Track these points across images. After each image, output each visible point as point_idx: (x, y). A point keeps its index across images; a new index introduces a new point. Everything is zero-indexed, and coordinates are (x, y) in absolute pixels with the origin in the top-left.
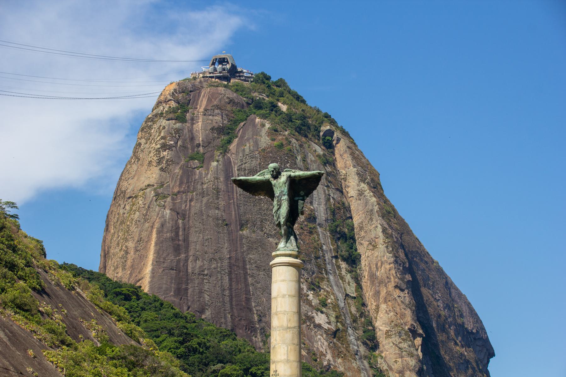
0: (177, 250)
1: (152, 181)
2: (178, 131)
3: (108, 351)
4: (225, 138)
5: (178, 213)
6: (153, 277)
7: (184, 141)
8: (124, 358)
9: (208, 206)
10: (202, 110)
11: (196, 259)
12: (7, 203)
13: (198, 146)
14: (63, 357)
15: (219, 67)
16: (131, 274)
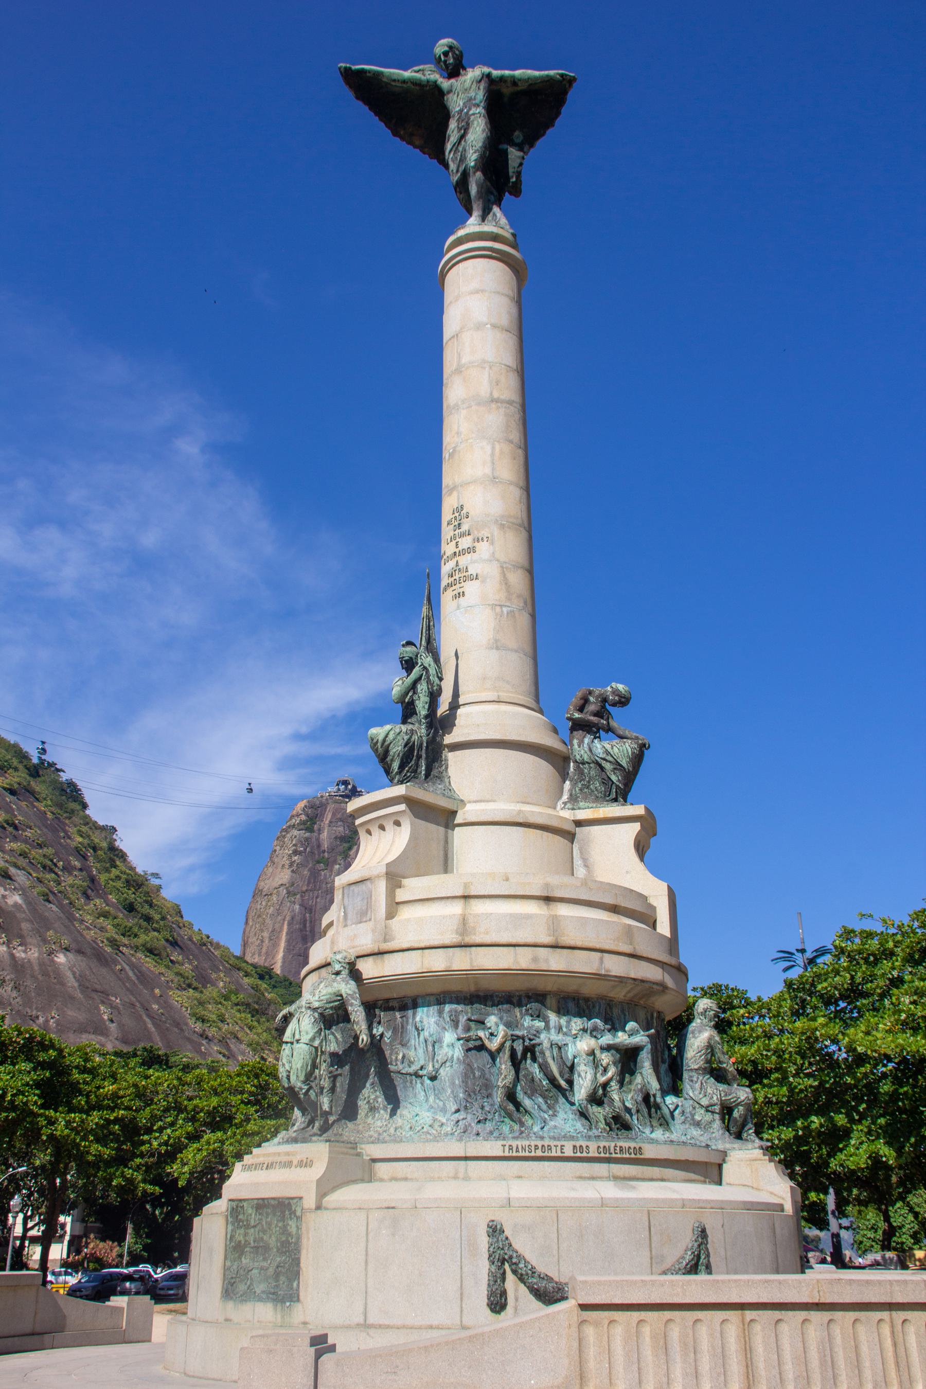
2: (307, 839)
3: (233, 997)
4: (346, 845)
6: (284, 962)
7: (312, 848)
10: (327, 822)
12: (153, 874)
13: (324, 852)
14: (188, 998)
15: (342, 787)
16: (266, 959)
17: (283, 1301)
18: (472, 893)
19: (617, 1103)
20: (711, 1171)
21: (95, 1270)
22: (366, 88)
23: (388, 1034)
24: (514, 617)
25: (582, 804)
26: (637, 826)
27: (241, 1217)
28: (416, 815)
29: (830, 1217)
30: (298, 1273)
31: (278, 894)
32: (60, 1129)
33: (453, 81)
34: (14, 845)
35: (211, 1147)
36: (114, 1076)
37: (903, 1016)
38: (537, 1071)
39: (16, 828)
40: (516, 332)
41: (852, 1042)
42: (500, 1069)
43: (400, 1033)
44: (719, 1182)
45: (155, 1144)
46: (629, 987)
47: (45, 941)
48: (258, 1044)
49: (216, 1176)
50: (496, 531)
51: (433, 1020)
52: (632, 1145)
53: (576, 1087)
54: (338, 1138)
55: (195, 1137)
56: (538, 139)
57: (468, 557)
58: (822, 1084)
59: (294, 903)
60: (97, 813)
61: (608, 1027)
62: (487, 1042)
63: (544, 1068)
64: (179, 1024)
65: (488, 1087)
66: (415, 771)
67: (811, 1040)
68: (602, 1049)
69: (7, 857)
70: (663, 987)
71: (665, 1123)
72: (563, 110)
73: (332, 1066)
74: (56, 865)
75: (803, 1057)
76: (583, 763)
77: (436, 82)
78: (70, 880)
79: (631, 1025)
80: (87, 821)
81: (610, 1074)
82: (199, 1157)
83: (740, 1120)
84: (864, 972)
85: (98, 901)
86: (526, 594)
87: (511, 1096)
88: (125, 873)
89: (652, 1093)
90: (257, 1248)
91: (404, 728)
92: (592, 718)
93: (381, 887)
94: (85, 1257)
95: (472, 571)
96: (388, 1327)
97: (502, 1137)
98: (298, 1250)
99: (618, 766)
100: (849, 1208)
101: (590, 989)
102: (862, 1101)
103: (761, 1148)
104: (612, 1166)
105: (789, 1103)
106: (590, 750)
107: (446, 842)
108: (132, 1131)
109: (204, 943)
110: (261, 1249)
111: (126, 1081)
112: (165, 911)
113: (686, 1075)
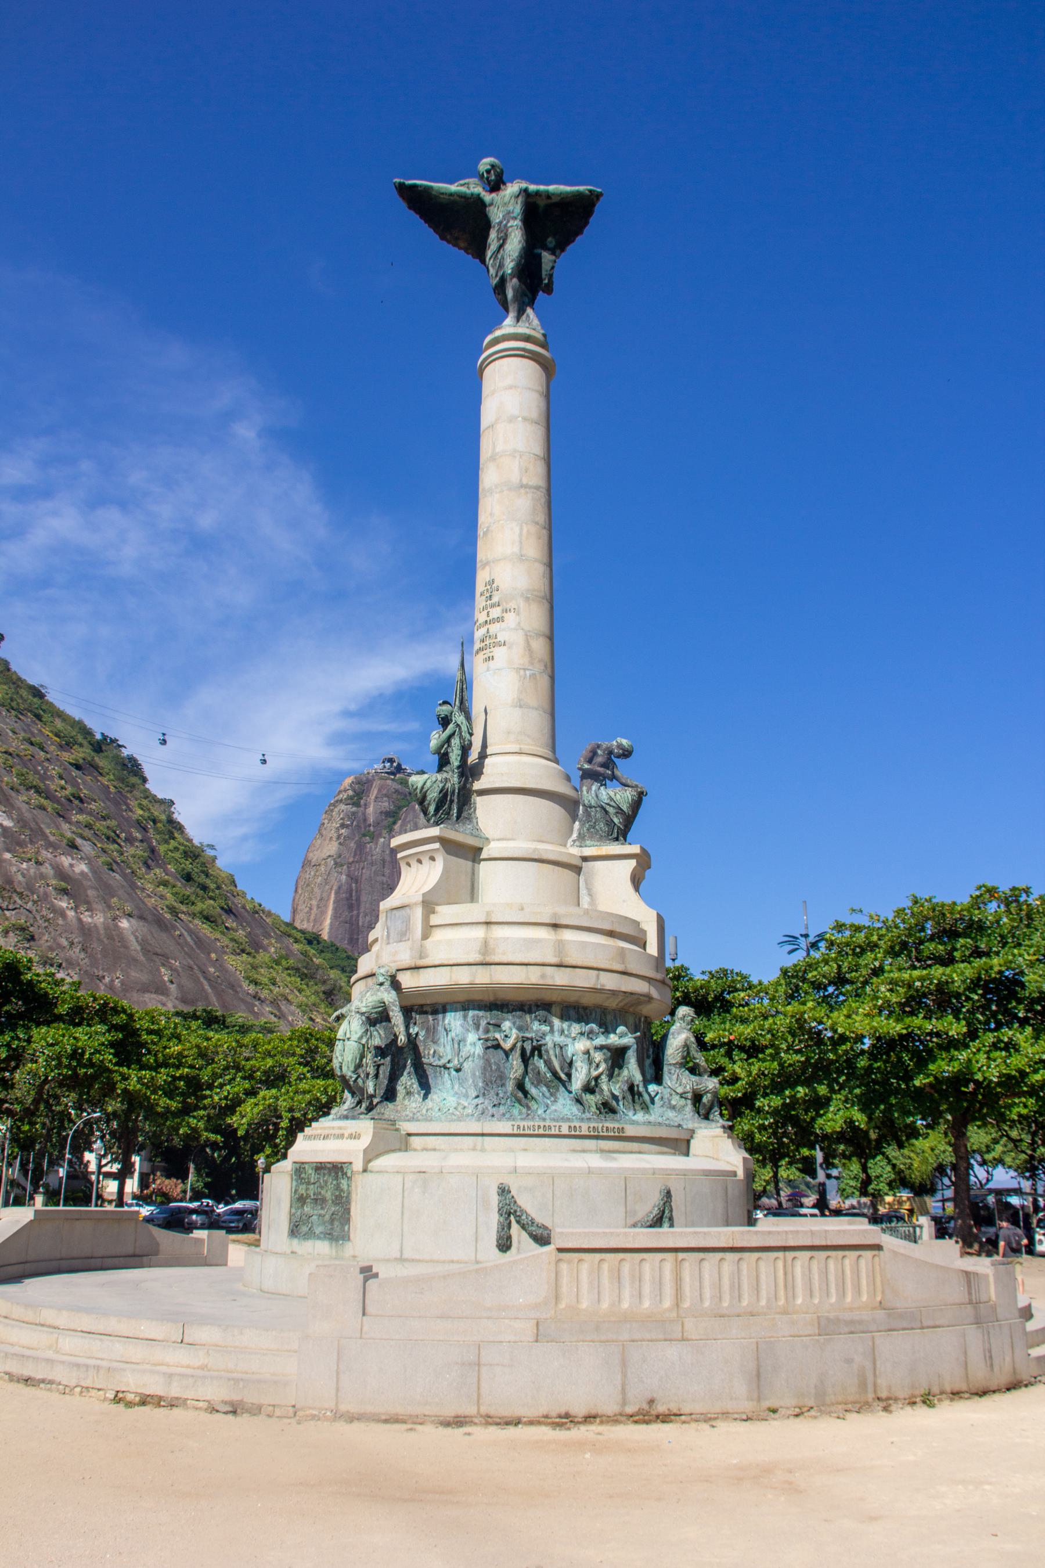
0: (351, 907)
1: (332, 853)
2: (354, 814)
3: (284, 962)
4: (391, 820)
5: (353, 878)
7: (358, 822)
8: (297, 970)
9: (376, 873)
11: (366, 915)
14: (242, 962)
15: (388, 765)
17: (337, 1240)
18: (493, 920)
19: (606, 1093)
20: (681, 1145)
21: (162, 1203)
22: (419, 201)
23: (422, 1033)
24: (535, 679)
25: (588, 843)
26: (633, 863)
27: (303, 1175)
28: (448, 852)
29: (819, 1168)
30: (349, 1220)
31: (326, 865)
32: (133, 1084)
33: (494, 195)
34: (81, 818)
35: (267, 1102)
36: (178, 1037)
37: (880, 1002)
38: (543, 1065)
39: (81, 801)
40: (544, 424)
41: (835, 1024)
42: (512, 1064)
43: (432, 1033)
44: (687, 1154)
45: (216, 1098)
46: (620, 998)
47: (110, 907)
48: (307, 1005)
49: (271, 1127)
50: (522, 603)
51: (459, 1023)
52: (617, 1125)
53: (573, 1079)
54: (380, 1116)
55: (252, 1093)
56: (568, 244)
57: (497, 625)
58: (808, 1059)
59: (341, 873)
60: (156, 787)
61: (602, 1030)
62: (502, 1043)
63: (548, 1063)
64: (233, 986)
65: (502, 1078)
66: (448, 814)
67: (801, 1022)
68: (596, 1048)
69: (74, 829)
70: (649, 998)
71: (645, 1108)
72: (591, 220)
73: (376, 1057)
74: (118, 836)
75: (794, 1035)
76: (591, 807)
77: (479, 195)
78: (132, 850)
79: (621, 1029)
80: (147, 795)
81: (601, 1070)
82: (256, 1110)
83: (708, 1105)
84: (850, 963)
85: (158, 871)
86: (547, 659)
87: (520, 1086)
88: (183, 845)
89: (636, 1083)
90: (316, 1200)
91: (439, 777)
92: (599, 769)
93: (418, 913)
94: (153, 1192)
95: (500, 638)
96: (419, 1261)
97: (512, 1118)
98: (348, 1202)
99: (619, 810)
100: (836, 1161)
101: (587, 1000)
102: (843, 1074)
103: (723, 1127)
104: (600, 1142)
105: (779, 1075)
106: (597, 796)
107: (473, 874)
108: (195, 1086)
109: (257, 911)
110: (319, 1201)
111: (189, 1042)
112: (220, 881)
113: (666, 1069)
